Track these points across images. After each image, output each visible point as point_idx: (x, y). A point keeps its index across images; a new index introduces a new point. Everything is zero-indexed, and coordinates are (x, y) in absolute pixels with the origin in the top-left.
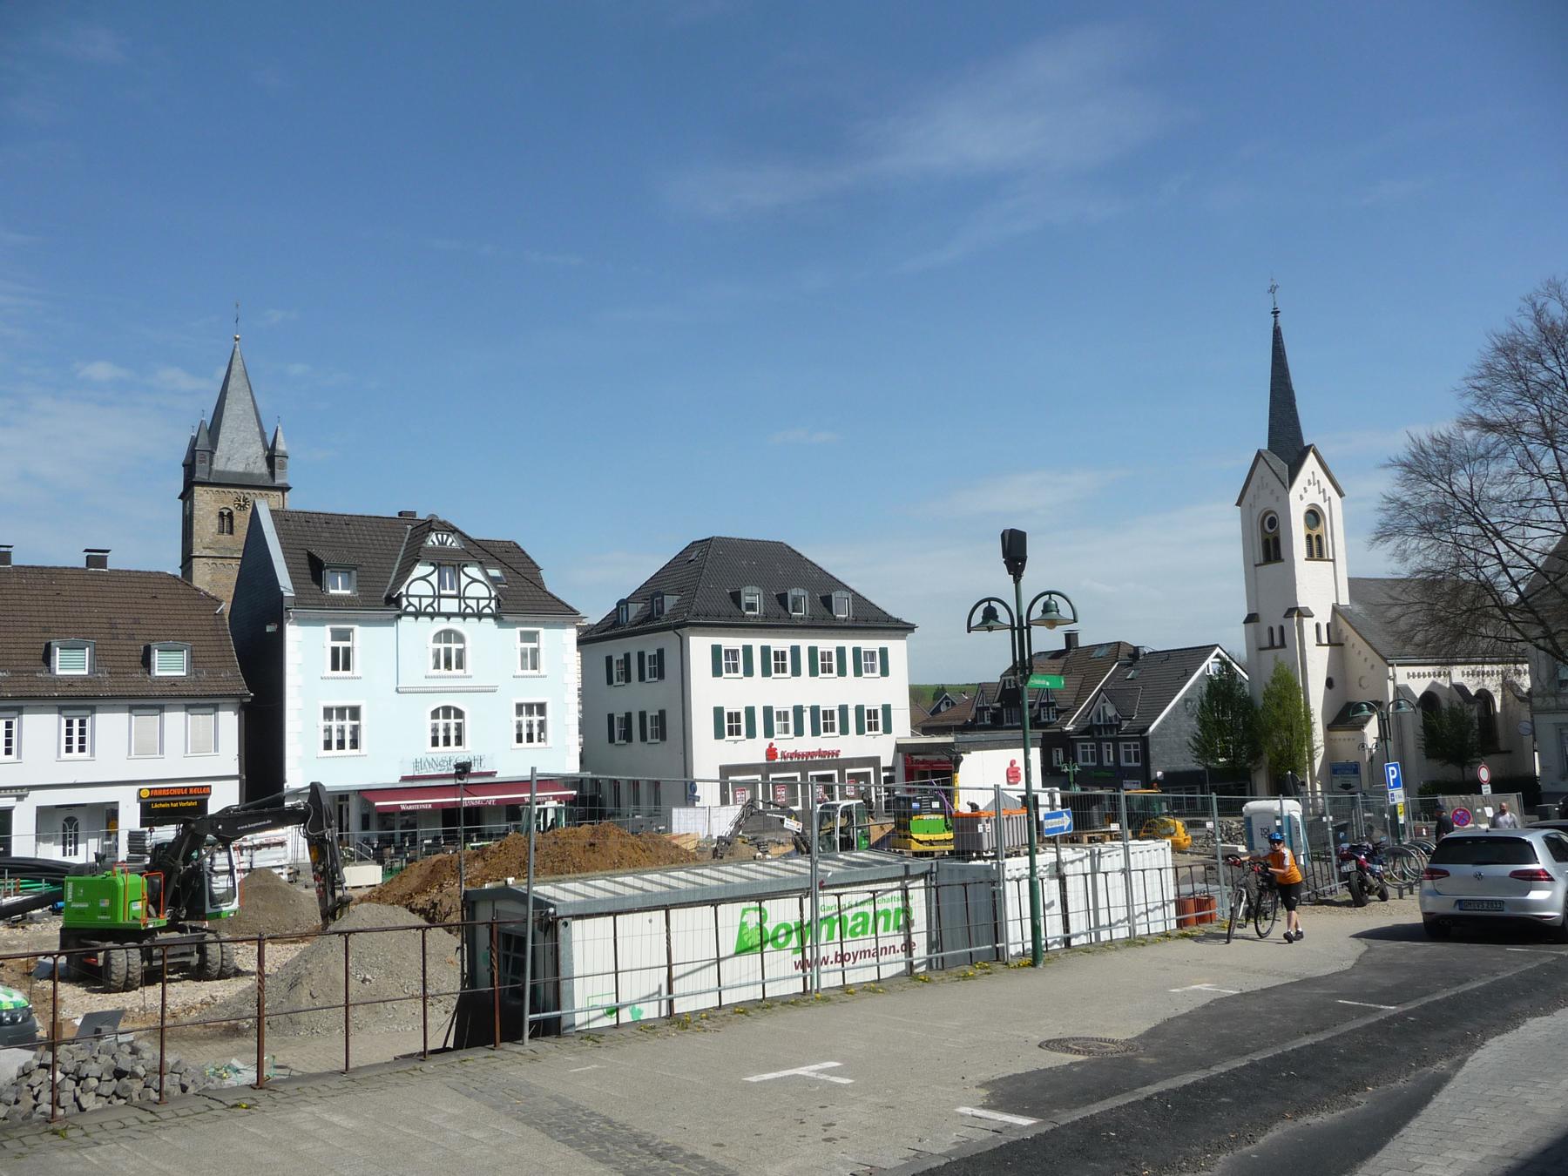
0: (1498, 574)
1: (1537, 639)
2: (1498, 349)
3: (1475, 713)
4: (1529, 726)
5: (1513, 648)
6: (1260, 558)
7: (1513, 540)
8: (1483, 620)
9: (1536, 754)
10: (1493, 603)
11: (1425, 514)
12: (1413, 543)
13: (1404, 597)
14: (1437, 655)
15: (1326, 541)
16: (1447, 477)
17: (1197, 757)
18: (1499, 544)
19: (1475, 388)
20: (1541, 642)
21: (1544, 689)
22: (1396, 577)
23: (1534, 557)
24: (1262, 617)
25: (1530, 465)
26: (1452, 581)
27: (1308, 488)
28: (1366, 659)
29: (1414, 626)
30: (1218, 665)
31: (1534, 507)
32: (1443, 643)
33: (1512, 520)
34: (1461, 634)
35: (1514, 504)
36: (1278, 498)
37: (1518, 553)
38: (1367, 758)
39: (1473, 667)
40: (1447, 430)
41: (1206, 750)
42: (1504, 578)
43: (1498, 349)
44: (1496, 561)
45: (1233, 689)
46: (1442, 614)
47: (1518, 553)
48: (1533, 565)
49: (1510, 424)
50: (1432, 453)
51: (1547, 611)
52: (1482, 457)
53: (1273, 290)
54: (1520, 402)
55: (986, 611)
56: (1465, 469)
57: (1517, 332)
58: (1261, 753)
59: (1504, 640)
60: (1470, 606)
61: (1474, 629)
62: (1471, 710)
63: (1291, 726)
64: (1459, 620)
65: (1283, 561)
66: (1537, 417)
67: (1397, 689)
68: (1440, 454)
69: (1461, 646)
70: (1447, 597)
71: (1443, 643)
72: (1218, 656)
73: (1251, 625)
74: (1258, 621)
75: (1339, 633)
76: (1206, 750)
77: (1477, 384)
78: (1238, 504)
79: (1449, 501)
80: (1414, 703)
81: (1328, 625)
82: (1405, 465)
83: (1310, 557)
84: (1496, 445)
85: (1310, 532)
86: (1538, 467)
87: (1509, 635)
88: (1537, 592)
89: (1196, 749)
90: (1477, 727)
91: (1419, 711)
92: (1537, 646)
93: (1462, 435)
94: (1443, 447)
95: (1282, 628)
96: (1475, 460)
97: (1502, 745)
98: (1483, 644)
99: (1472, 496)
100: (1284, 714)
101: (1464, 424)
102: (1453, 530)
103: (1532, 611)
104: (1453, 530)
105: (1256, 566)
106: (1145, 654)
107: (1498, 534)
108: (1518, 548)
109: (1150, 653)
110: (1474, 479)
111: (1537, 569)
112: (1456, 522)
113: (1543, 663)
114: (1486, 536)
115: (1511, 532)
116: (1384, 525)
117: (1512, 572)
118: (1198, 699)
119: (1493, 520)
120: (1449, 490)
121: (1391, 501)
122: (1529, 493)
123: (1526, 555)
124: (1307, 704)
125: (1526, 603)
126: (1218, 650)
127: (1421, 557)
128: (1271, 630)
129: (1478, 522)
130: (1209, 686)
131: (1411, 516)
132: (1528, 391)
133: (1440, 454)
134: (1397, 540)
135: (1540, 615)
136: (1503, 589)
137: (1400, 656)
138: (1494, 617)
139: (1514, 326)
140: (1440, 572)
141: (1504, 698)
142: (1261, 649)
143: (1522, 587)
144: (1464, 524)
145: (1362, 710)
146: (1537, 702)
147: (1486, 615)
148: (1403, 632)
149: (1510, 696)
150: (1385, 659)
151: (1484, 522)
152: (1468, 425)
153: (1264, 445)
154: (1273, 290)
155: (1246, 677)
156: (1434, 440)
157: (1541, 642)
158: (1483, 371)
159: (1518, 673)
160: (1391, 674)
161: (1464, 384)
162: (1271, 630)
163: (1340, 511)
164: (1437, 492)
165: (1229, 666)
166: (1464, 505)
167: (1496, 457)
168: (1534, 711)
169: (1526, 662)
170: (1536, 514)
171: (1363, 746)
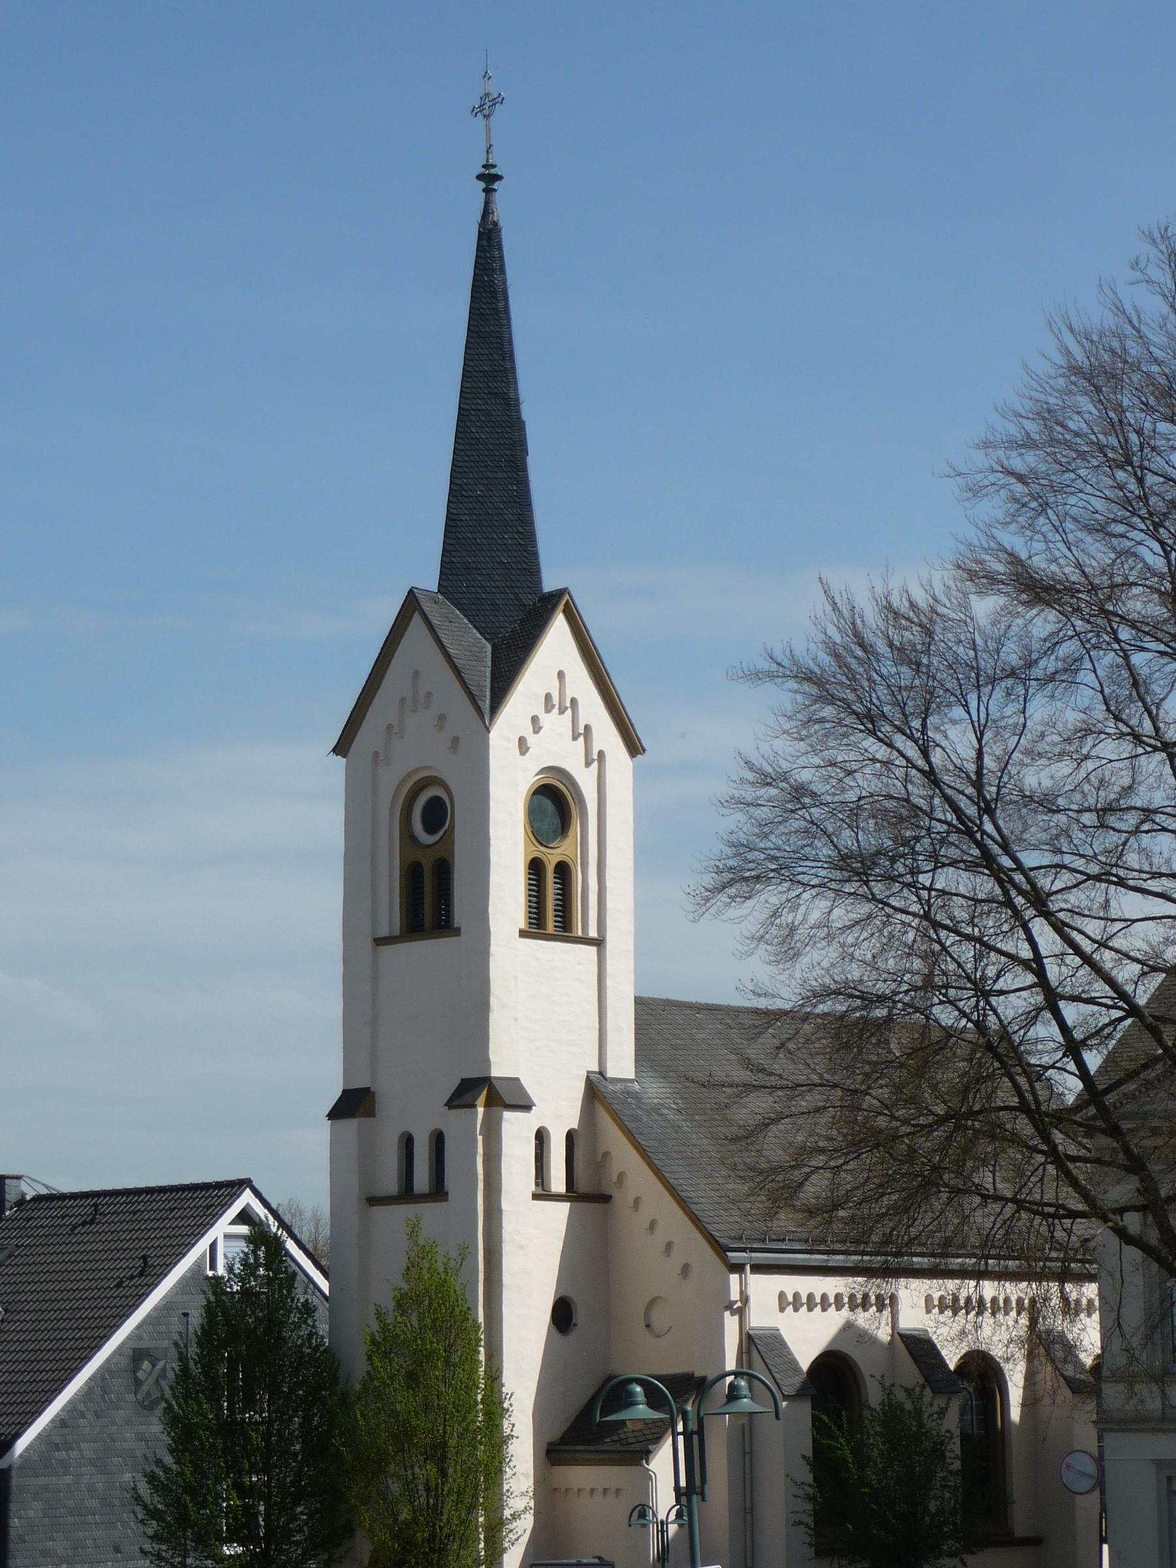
0: (1031, 1018)
1: (1121, 1211)
2: (1075, 370)
3: (952, 1422)
4: (1091, 1468)
5: (1059, 1234)
6: (390, 918)
7: (1078, 922)
8: (985, 1147)
9: (1105, 1547)
10: (1015, 1101)
11: (855, 828)
12: (814, 908)
13: (782, 1065)
14: (859, 1243)
15: (586, 882)
16: (916, 724)
17: (156, 1538)
18: (1041, 929)
19: (1011, 473)
20: (1133, 1222)
21: (1133, 1359)
22: (762, 1003)
23: (1126, 973)
24: (385, 1103)
25: (1135, 713)
26: (911, 1027)
27: (546, 720)
28: (669, 1247)
29: (803, 1153)
30: (242, 1246)
31: (1137, 831)
32: (878, 1208)
33: (1079, 863)
34: (928, 1184)
35: (1088, 819)
36: (456, 740)
37: (1087, 960)
38: (653, 1552)
39: (951, 1284)
40: (928, 588)
41: (183, 1521)
42: (1046, 1030)
43: (1075, 370)
44: (1030, 979)
45: (281, 1324)
46: (882, 1122)
47: (1087, 960)
48: (1122, 995)
49: (1094, 589)
50: (882, 647)
51: (1155, 1131)
52: (1012, 673)
53: (487, 107)
54: (1120, 529)
55: (640, 1511)
56: (966, 706)
57: (1129, 330)
58: (348, 1531)
59: (1036, 1209)
60: (954, 1103)
61: (958, 1174)
62: (942, 1413)
63: (444, 1445)
64: (925, 1144)
65: (457, 932)
66: (1162, 577)
67: (749, 1342)
68: (903, 654)
69: (924, 1219)
70: (897, 1075)
71: (878, 1208)
72: (245, 1217)
73: (351, 1125)
74: (371, 1113)
75: (600, 1162)
76: (183, 1521)
77: (1017, 463)
78: (342, 748)
79: (919, 793)
80: (791, 1384)
81: (570, 1136)
82: (808, 677)
83: (536, 927)
84: (1053, 643)
85: (539, 851)
86: (1154, 720)
87: (1049, 1196)
88: (1131, 1075)
89: (153, 1514)
90: (957, 1465)
91: (805, 1410)
92: (1122, 1234)
93: (965, 607)
94: (913, 636)
95: (438, 1140)
96: (993, 681)
97: (1020, 1521)
98: (984, 1218)
99: (978, 784)
100: (427, 1408)
101: (972, 575)
102: (925, 879)
103: (1114, 1131)
104: (925, 879)
105: (379, 942)
106: (21, 1202)
107: (1039, 901)
108: (1087, 946)
109: (38, 1199)
110: (988, 735)
111: (1133, 1011)
112: (934, 856)
113: (1136, 1284)
114: (1009, 903)
115: (1075, 898)
116: (741, 848)
117: (1070, 1012)
118: (173, 1352)
119: (1030, 859)
120: (921, 762)
121: (766, 780)
122: (1129, 790)
123: (1108, 966)
124: (494, 1377)
125: (1101, 1107)
126: (247, 1198)
127: (833, 953)
128: (408, 1142)
129: (987, 862)
130: (210, 1310)
131: (814, 829)
132: (1145, 498)
133: (903, 654)
134: (772, 895)
135: (1133, 1142)
136: (1046, 1060)
137: (763, 1241)
138: (1015, 1139)
139: (1120, 310)
140: (881, 999)
141: (1030, 1378)
142: (373, 1201)
143: (1093, 1060)
144: (954, 863)
145: (630, 1403)
146: (1113, 1394)
147: (996, 1133)
148: (774, 1170)
149: (1046, 1372)
150: (721, 1250)
151: (1006, 862)
152: (987, 581)
153: (428, 579)
154: (487, 107)
155: (324, 1285)
156: (891, 612)
157: (1133, 1222)
158: (1033, 428)
159: (1070, 1309)
160: (735, 1295)
161: (980, 459)
162: (408, 1142)
163: (629, 796)
164: (887, 764)
165: (275, 1248)
166: (956, 809)
167: (1051, 678)
168: (1106, 1423)
169: (1091, 1278)
170: (1141, 850)
171: (642, 1511)
